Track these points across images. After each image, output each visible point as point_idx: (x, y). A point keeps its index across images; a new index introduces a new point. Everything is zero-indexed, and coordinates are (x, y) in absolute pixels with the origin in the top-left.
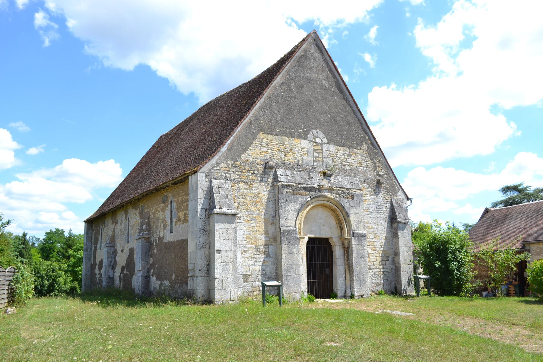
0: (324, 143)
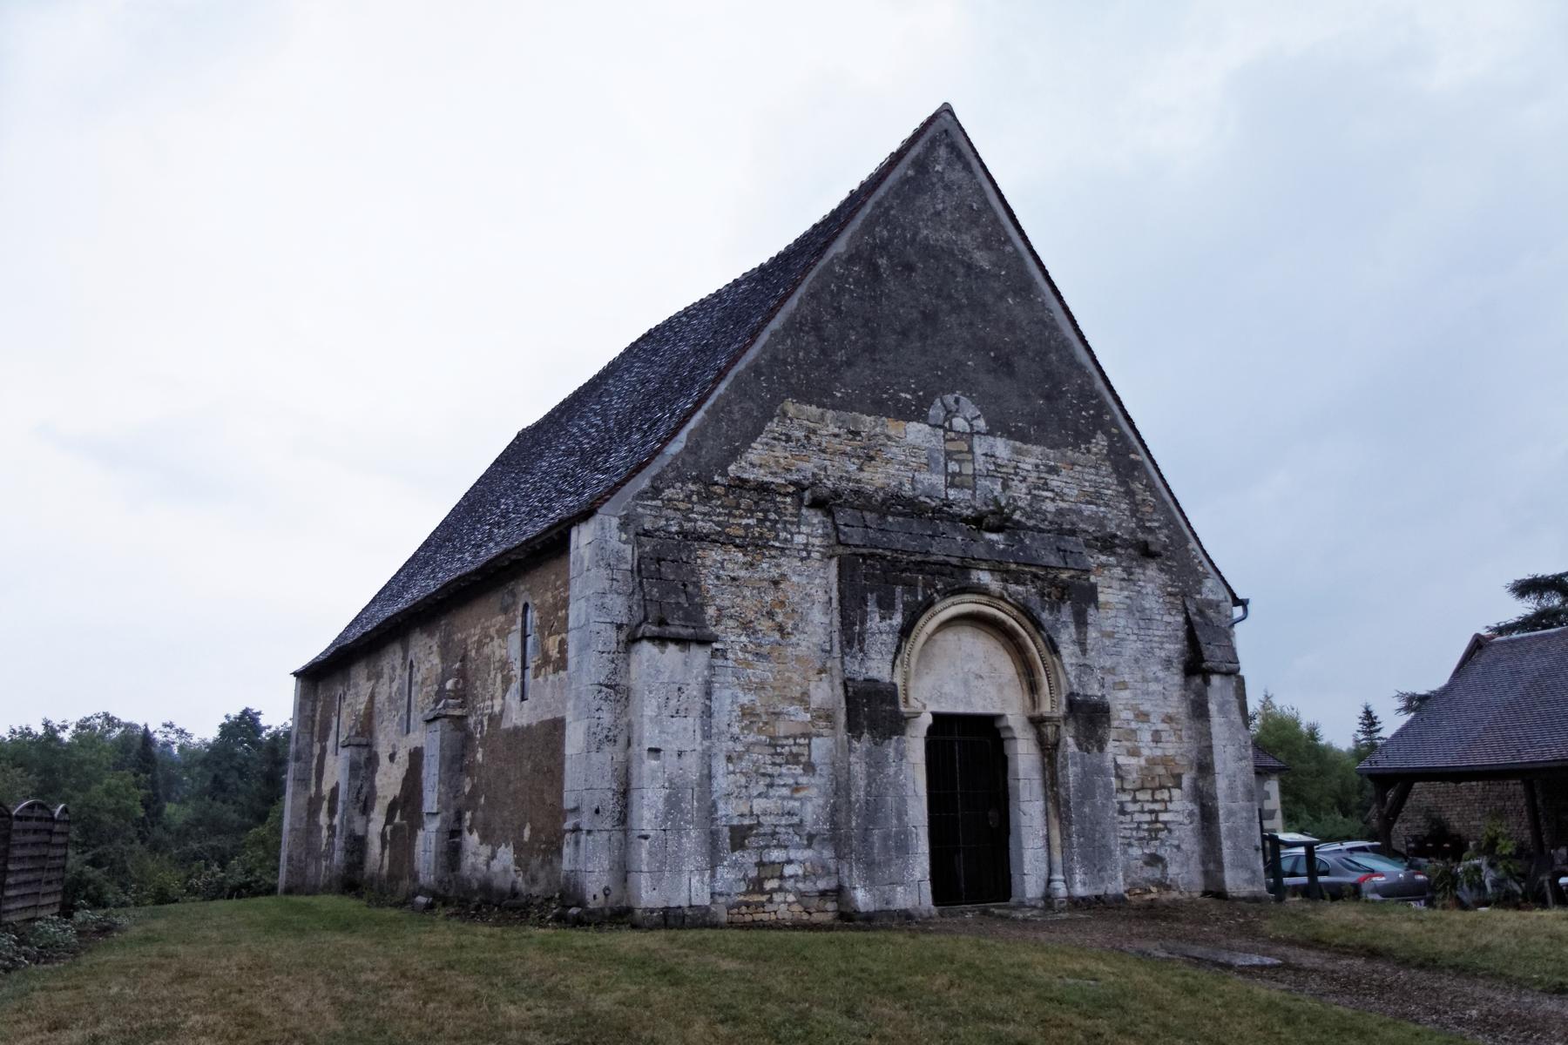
0: (978, 433)
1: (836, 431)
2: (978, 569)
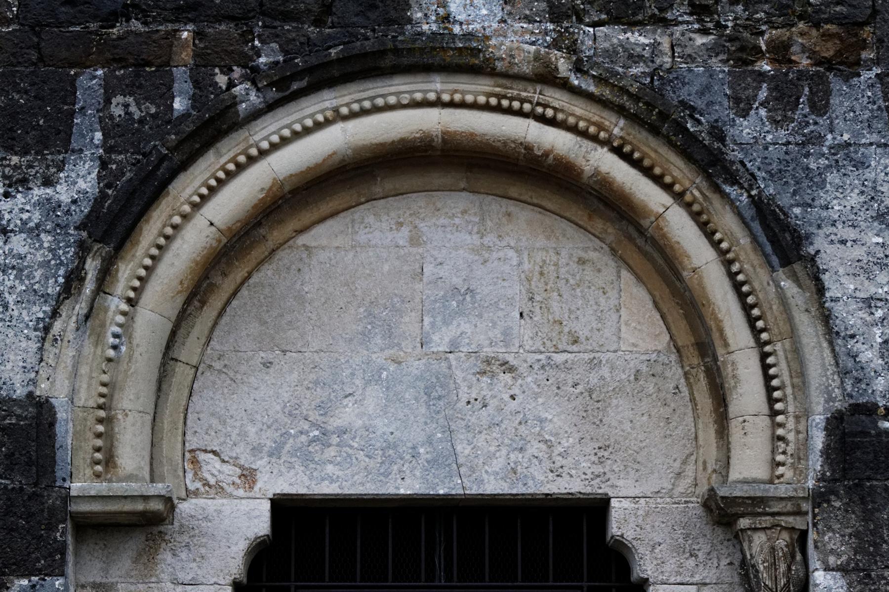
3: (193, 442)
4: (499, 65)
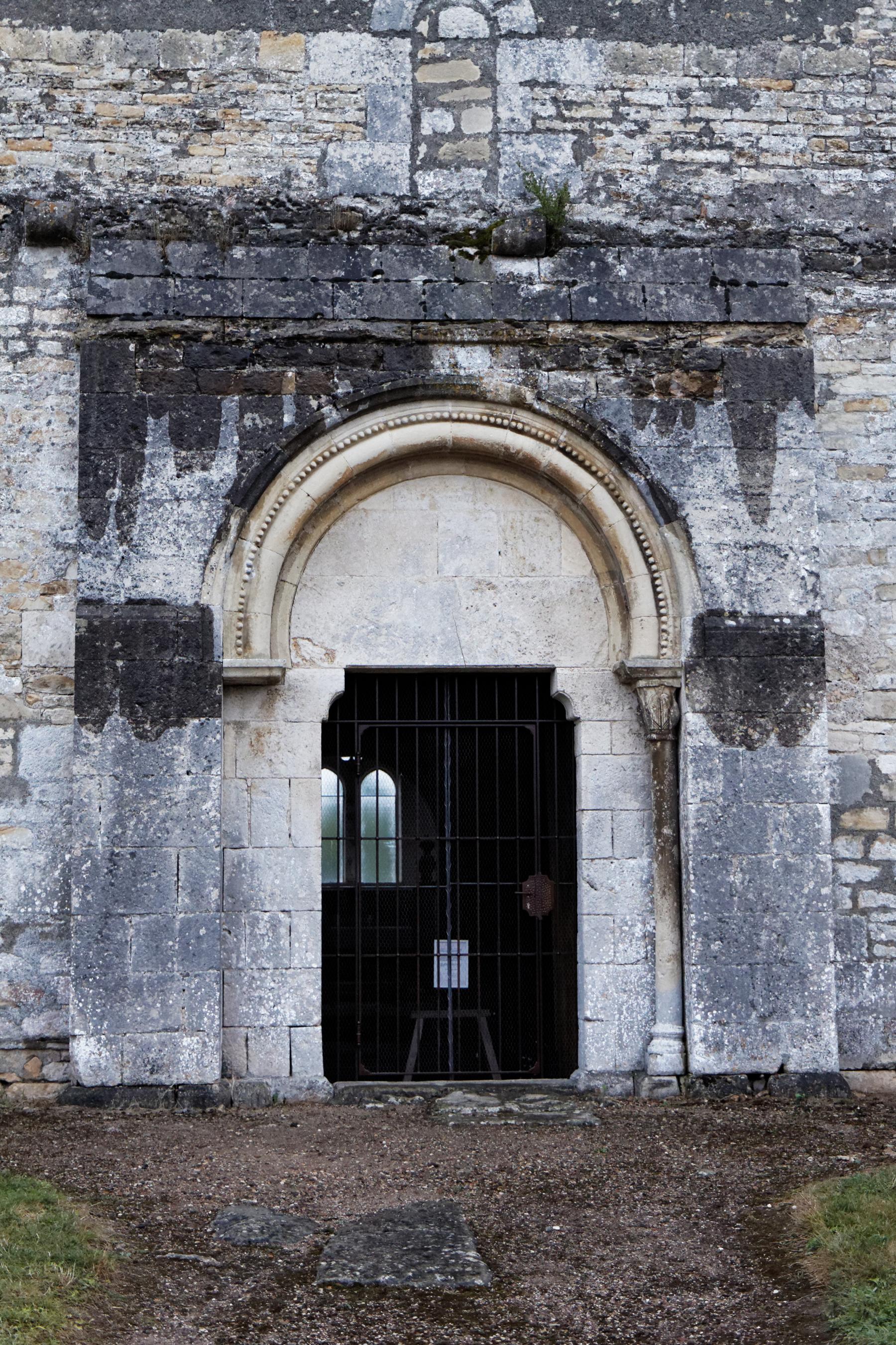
0: (511, 34)
1: (123, 75)
2: (454, 343)
3: (295, 633)
4: (489, 395)
